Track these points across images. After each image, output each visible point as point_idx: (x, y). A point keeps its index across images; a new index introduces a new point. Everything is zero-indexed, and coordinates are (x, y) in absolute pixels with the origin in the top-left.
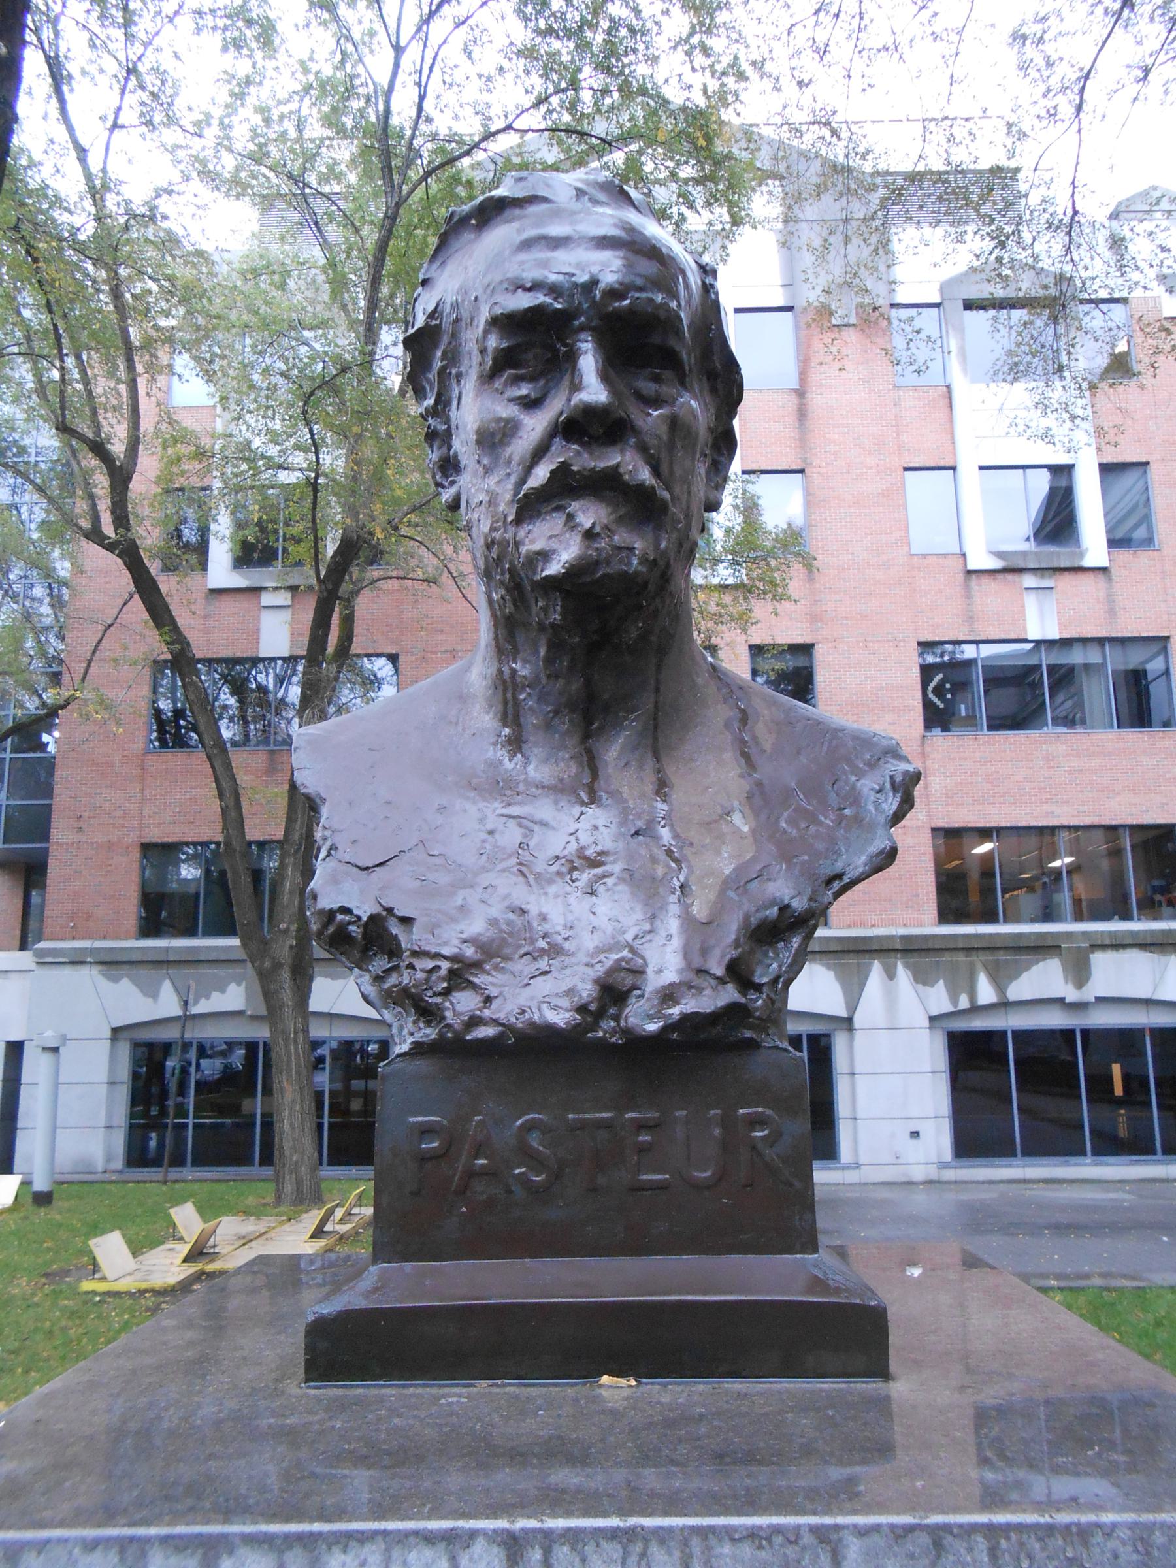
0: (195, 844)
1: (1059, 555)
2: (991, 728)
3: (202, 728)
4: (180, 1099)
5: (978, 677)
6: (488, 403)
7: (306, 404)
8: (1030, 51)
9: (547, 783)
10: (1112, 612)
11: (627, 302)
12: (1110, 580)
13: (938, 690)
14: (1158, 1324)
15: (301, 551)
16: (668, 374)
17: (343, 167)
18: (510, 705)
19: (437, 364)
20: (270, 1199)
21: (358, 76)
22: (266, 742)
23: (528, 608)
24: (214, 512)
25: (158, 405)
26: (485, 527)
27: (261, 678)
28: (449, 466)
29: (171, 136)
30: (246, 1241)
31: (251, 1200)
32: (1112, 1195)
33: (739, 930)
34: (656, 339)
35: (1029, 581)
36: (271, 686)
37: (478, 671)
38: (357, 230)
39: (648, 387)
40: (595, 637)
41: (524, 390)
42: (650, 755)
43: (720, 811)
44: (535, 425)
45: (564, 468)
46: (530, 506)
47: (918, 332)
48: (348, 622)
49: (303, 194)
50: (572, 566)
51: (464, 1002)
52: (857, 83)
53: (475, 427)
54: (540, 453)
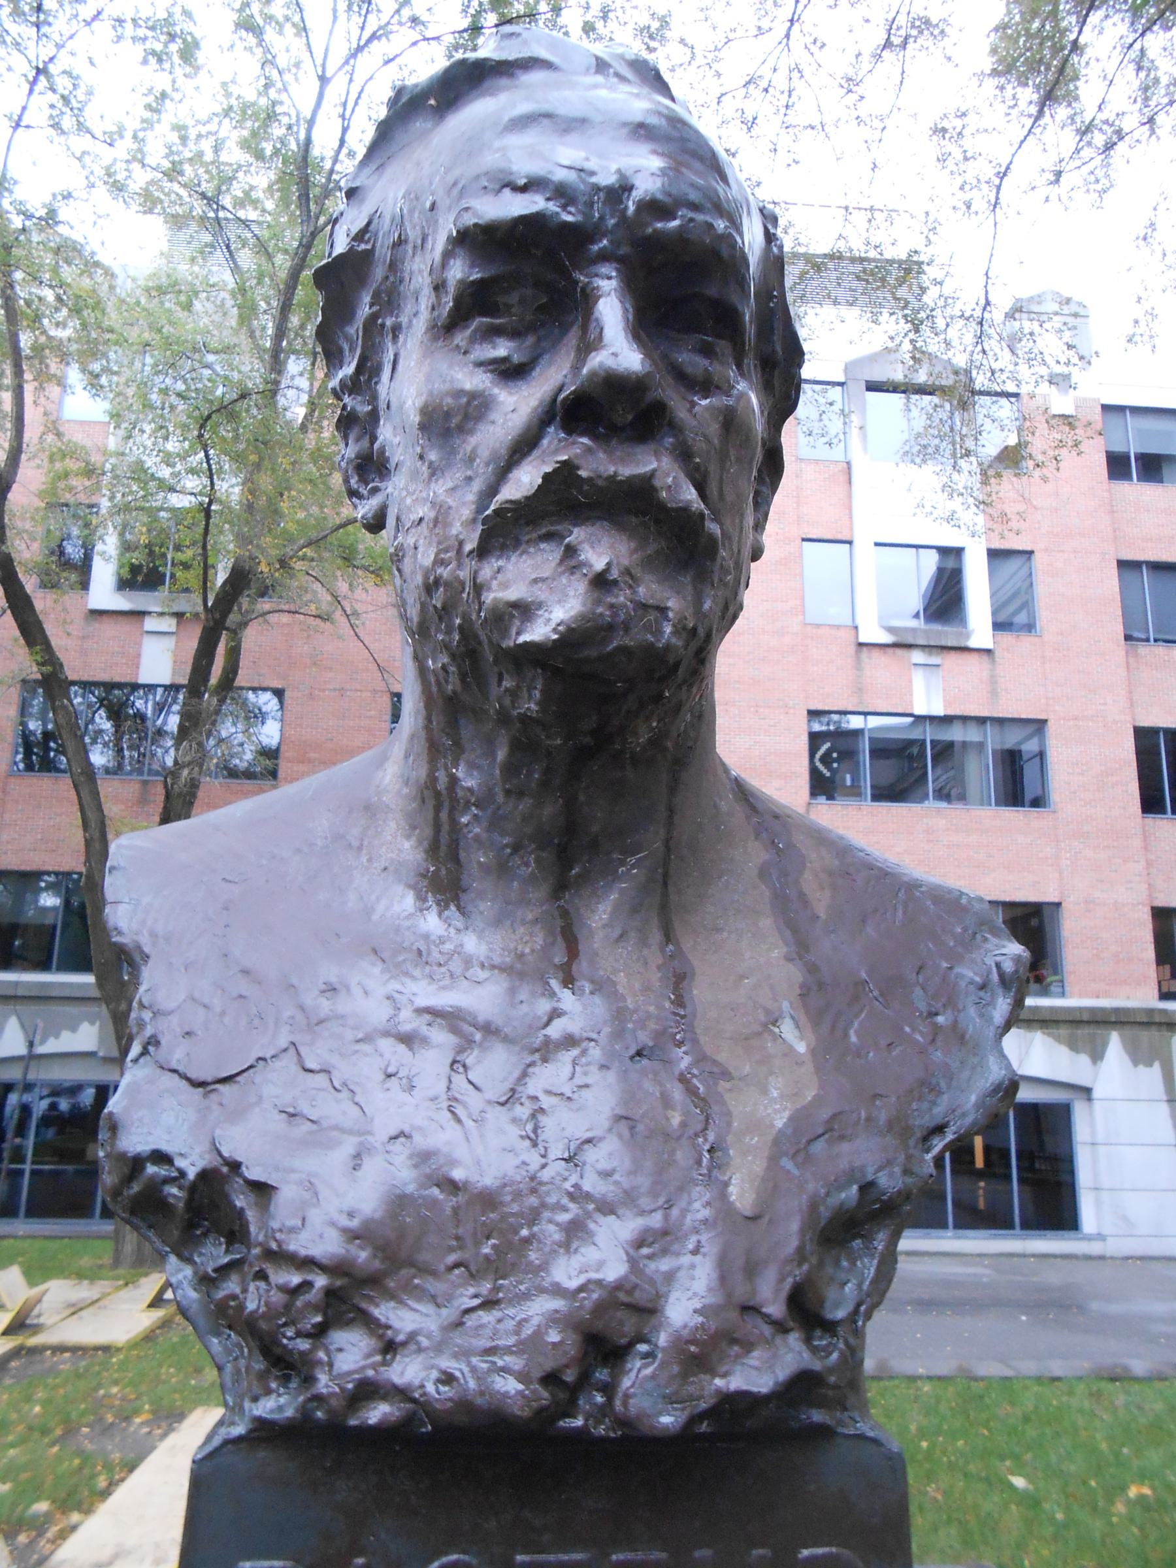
0: (57, 874)
1: (946, 633)
2: (876, 797)
3: (70, 754)
4: (18, 1140)
5: (866, 746)
6: (443, 367)
7: (202, 426)
8: (949, 147)
9: (497, 960)
10: (994, 693)
11: (675, 223)
12: (993, 661)
13: (826, 759)
14: (1026, 1419)
15: (191, 578)
16: (723, 346)
17: (261, 195)
18: (446, 828)
19: (364, 310)
20: (107, 1259)
21: (281, 103)
22: (140, 772)
23: (482, 686)
24: (101, 531)
25: (45, 414)
26: (426, 557)
27: (139, 704)
28: (371, 467)
29: (80, 143)
30: (76, 1309)
31: (86, 1261)
32: (971, 1270)
33: (802, 1232)
34: (712, 291)
35: (918, 657)
36: (149, 713)
37: (390, 766)
38: (270, 257)
39: (692, 361)
40: (588, 740)
41: (502, 349)
42: (655, 922)
43: (762, 1017)
44: (516, 406)
45: (567, 469)
46: (504, 530)
47: (831, 404)
48: (234, 654)
49: (217, 219)
50: (570, 630)
51: (350, 1352)
52: (783, 157)
53: (419, 403)
54: (523, 447)
